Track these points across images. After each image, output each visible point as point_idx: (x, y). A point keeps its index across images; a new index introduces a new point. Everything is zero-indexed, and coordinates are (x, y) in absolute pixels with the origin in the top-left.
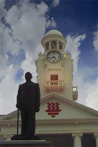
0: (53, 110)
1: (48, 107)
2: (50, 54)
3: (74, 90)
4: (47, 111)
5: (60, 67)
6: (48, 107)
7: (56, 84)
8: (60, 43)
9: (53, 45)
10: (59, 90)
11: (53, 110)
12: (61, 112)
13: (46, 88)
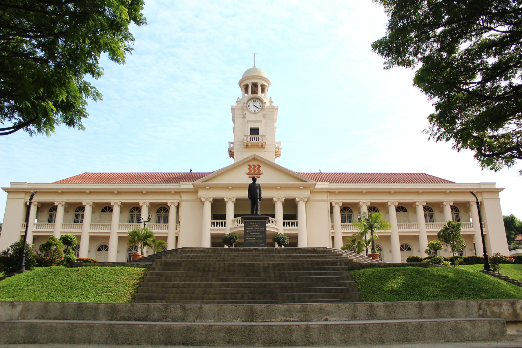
0: (254, 173)
1: (260, 171)
2: (250, 102)
3: (277, 145)
4: (248, 174)
5: (262, 119)
6: (249, 169)
7: (257, 139)
8: (262, 86)
9: (254, 88)
10: (260, 146)
11: (254, 173)
12: (262, 175)
13: (245, 144)
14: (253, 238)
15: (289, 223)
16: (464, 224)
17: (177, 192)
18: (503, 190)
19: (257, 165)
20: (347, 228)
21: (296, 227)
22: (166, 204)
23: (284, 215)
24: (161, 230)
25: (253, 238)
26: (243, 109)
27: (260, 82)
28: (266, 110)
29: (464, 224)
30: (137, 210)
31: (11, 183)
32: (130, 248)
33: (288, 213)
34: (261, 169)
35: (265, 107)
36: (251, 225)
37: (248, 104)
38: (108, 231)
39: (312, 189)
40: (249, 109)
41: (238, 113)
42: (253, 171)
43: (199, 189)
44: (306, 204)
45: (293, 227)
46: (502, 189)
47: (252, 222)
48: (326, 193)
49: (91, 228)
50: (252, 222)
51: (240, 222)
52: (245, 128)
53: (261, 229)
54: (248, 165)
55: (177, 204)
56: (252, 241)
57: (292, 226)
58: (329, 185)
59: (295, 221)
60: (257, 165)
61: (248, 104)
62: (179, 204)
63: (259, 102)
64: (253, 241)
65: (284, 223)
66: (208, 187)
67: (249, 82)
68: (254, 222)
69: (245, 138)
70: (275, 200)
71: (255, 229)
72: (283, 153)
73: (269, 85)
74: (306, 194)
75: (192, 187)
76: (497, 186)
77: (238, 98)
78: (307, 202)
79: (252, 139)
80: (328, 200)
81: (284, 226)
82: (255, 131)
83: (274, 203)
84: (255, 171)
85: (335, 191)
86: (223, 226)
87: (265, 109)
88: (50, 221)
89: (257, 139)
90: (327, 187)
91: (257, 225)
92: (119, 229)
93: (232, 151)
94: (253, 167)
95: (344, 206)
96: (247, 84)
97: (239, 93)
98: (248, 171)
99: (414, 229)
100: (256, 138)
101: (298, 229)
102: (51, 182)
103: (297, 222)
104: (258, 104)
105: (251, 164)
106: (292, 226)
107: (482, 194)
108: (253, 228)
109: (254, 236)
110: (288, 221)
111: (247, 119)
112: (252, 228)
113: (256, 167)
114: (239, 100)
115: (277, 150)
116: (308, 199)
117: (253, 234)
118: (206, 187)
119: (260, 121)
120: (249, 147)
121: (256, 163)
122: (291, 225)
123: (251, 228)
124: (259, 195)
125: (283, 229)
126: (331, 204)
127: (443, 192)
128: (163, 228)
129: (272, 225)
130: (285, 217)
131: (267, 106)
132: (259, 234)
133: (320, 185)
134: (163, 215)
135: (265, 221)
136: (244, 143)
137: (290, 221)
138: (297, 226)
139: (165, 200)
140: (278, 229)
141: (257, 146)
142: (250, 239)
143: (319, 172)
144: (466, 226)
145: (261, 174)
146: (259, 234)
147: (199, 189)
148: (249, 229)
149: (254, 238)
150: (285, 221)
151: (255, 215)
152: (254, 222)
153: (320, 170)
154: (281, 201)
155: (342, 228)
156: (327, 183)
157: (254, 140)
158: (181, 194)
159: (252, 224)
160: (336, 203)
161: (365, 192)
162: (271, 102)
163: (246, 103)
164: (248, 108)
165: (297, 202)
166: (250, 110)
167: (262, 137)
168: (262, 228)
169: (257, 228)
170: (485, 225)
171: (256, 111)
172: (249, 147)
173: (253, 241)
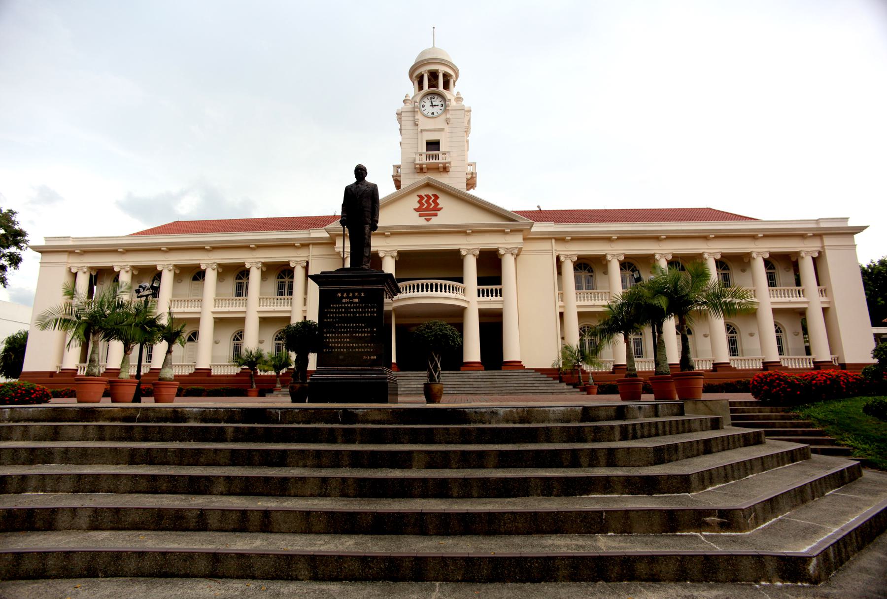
3: (470, 169)
6: (420, 202)
7: (437, 157)
10: (441, 170)
11: (427, 209)
15: (492, 290)
16: (784, 290)
17: (305, 245)
18: (865, 231)
19: (433, 195)
20: (586, 298)
21: (499, 298)
22: (287, 264)
23: (478, 278)
24: (284, 306)
26: (414, 111)
27: (442, 69)
28: (451, 112)
29: (784, 290)
31: (45, 238)
32: (238, 336)
34: (438, 201)
35: (449, 106)
37: (423, 103)
38: (289, 308)
41: (407, 119)
42: (426, 205)
43: (337, 238)
44: (516, 259)
45: (494, 298)
46: (860, 229)
48: (550, 241)
49: (261, 304)
50: (343, 291)
51: (406, 290)
52: (418, 136)
53: (368, 312)
54: (418, 196)
56: (341, 348)
57: (492, 296)
59: (498, 287)
60: (433, 195)
62: (308, 263)
63: (439, 99)
64: (343, 348)
65: (479, 290)
67: (424, 70)
69: (417, 157)
71: (350, 313)
72: (479, 181)
73: (457, 75)
74: (516, 240)
75: (327, 235)
76: (851, 223)
81: (479, 296)
82: (433, 145)
84: (429, 204)
86: (485, 297)
87: (449, 110)
88: (239, 294)
91: (356, 300)
92: (260, 306)
93: (398, 178)
94: (426, 198)
95: (580, 261)
96: (421, 73)
97: (410, 88)
98: (417, 206)
99: (602, 300)
101: (503, 301)
102: (124, 235)
103: (501, 290)
105: (423, 193)
106: (492, 296)
107: (822, 239)
108: (345, 308)
109: (347, 332)
110: (485, 287)
111: (420, 128)
112: (342, 308)
113: (431, 198)
114: (408, 98)
115: (470, 176)
116: (520, 250)
117: (344, 328)
119: (442, 130)
120: (424, 170)
121: (430, 192)
122: (490, 295)
123: (339, 308)
125: (478, 302)
126: (558, 258)
127: (752, 236)
130: (481, 281)
132: (362, 328)
133: (539, 227)
134: (287, 282)
136: (415, 164)
138: (501, 296)
141: (436, 169)
142: (335, 343)
143: (538, 209)
144: (788, 294)
145: (440, 209)
146: (362, 328)
147: (337, 238)
148: (332, 313)
149: (347, 337)
150: (481, 287)
152: (348, 291)
153: (538, 207)
154: (474, 255)
155: (577, 298)
156: (552, 224)
158: (311, 246)
159: (342, 297)
160: (567, 257)
161: (616, 237)
162: (459, 99)
163: (418, 101)
164: (423, 109)
166: (425, 112)
167: (444, 154)
169: (356, 308)
170: (805, 292)
172: (425, 170)
173: (343, 348)
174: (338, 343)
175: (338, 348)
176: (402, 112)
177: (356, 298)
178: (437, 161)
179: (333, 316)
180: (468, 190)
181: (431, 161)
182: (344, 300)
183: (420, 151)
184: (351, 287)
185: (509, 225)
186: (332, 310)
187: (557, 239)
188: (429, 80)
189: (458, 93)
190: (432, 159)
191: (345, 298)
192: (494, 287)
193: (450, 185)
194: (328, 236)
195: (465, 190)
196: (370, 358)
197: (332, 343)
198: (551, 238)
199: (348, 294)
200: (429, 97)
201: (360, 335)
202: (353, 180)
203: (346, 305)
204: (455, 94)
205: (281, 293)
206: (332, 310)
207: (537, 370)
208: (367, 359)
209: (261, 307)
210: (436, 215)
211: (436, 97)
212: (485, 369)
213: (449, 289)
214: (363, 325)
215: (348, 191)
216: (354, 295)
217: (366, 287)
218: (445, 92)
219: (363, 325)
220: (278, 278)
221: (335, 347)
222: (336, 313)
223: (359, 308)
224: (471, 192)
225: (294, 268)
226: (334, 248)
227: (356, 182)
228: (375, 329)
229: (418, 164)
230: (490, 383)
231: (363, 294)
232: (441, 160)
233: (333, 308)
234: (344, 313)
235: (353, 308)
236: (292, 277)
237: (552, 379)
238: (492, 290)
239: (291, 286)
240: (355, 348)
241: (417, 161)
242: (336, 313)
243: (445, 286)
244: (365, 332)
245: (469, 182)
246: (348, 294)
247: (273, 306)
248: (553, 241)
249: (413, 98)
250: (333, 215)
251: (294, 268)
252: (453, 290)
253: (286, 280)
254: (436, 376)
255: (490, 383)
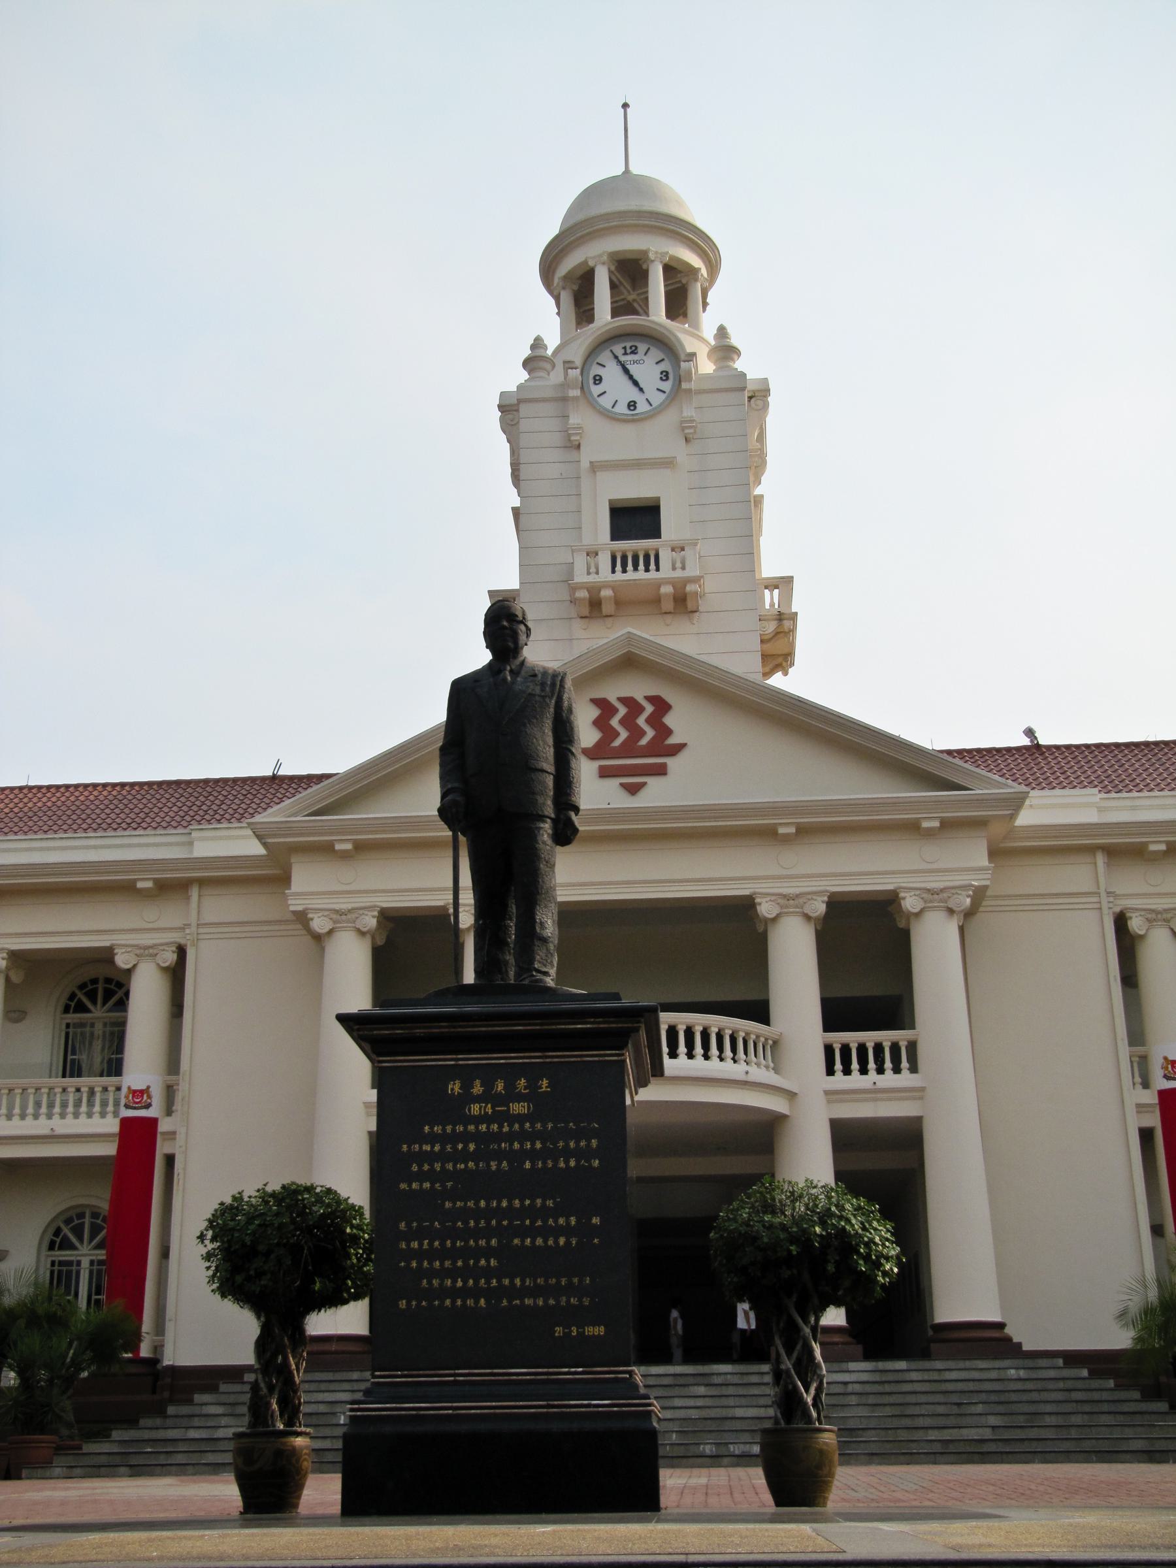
1: (668, 732)
3: (770, 599)
7: (650, 560)
8: (670, 270)
10: (668, 605)
11: (627, 748)
13: (583, 594)
14: (478, 1253)
19: (648, 698)
21: (906, 1079)
25: (478, 1253)
26: (564, 399)
30: (108, 994)
33: (852, 989)
34: (669, 720)
35: (690, 380)
36: (454, 1110)
37: (596, 370)
39: (997, 829)
40: (601, 400)
43: (294, 859)
44: (962, 930)
45: (889, 1079)
47: (467, 1075)
53: (567, 1154)
55: (170, 958)
58: (1101, 810)
60: (648, 698)
61: (596, 370)
62: (181, 952)
63: (656, 355)
64: (476, 1293)
65: (829, 1050)
66: (349, 846)
68: (488, 1074)
69: (580, 562)
70: (766, 909)
73: (714, 266)
75: (257, 849)
77: (538, 344)
78: (969, 914)
79: (620, 561)
80: (1104, 900)
83: (761, 929)
84: (637, 733)
85: (1146, 844)
89: (650, 560)
90: (1090, 817)
91: (518, 1108)
96: (585, 262)
100: (647, 557)
101: (923, 1089)
103: (912, 1047)
104: (647, 369)
108: (477, 1137)
109: (488, 1233)
110: (853, 1038)
111: (586, 457)
112: (466, 1137)
114: (539, 352)
115: (771, 627)
116: (979, 895)
117: (477, 1214)
118: (338, 847)
119: (668, 463)
123: (454, 1138)
124: (550, 781)
126: (1121, 922)
128: (64, 1105)
129: (753, 1069)
131: (707, 377)
132: (545, 1212)
135: (610, 1056)
136: (573, 589)
137: (870, 1038)
138: (914, 1069)
139: (70, 933)
140: (791, 1095)
142: (443, 1273)
143: (1026, 741)
146: (545, 1212)
147: (294, 859)
148: (431, 1157)
149: (488, 1253)
150: (839, 1038)
151: (467, 990)
153: (1030, 732)
154: (808, 918)
156: (1092, 795)
157: (630, 567)
158: (194, 892)
159: (467, 1098)
162: (725, 350)
163: (578, 362)
164: (596, 390)
165: (909, 916)
166: (605, 402)
167: (679, 548)
168: (578, 1135)
169: (522, 1136)
171: (642, 407)
173: (476, 1293)
174: (453, 1273)
175: (454, 1293)
176: (520, 401)
177: (520, 1098)
178: (653, 574)
179: (432, 1170)
180: (768, 674)
181: (631, 575)
182: (475, 1109)
183: (587, 540)
184: (499, 1059)
185: (938, 802)
186: (427, 1148)
187: (1114, 853)
188: (613, 286)
189: (722, 332)
190: (636, 568)
191: (478, 1099)
192: (886, 1037)
193: (715, 661)
194: (261, 851)
195: (757, 678)
196: (581, 1335)
197: (431, 1274)
198: (1091, 850)
199: (488, 1085)
200: (618, 349)
201: (539, 1241)
202: (480, 657)
203: (483, 1127)
204: (708, 331)
205: (71, 1069)
206: (427, 1148)
207: (1073, 1358)
208: (567, 1335)
209: (16, 1119)
210: (661, 771)
211: (642, 347)
212: (868, 1356)
213: (720, 1048)
214: (550, 1203)
215: (462, 691)
216: (510, 1086)
217: (555, 1057)
218: (678, 330)
219: (550, 1203)
220: (67, 1010)
221: (443, 1293)
222: (442, 1157)
223: (533, 1136)
224: (777, 681)
225: (129, 972)
226: (285, 897)
227: (490, 664)
228: (596, 1220)
229: (581, 586)
230: (896, 1411)
231: (545, 1082)
232: (666, 572)
233: (432, 1139)
234: (475, 1157)
235: (511, 1137)
236: (122, 1004)
237: (1136, 1395)
238: (862, 1049)
239: (117, 1039)
240: (524, 1292)
241: (580, 577)
242: (442, 1157)
243: (705, 1035)
244: (557, 1232)
245: (770, 648)
246: (488, 1085)
247: (50, 1116)
248: (1100, 859)
249: (557, 351)
250: (268, 773)
251: (129, 972)
252: (734, 1049)
253: (99, 1013)
254: (809, 1400)
255: (896, 1411)
